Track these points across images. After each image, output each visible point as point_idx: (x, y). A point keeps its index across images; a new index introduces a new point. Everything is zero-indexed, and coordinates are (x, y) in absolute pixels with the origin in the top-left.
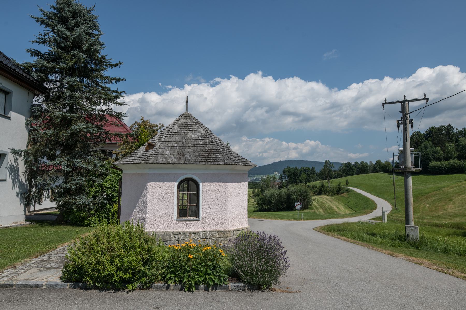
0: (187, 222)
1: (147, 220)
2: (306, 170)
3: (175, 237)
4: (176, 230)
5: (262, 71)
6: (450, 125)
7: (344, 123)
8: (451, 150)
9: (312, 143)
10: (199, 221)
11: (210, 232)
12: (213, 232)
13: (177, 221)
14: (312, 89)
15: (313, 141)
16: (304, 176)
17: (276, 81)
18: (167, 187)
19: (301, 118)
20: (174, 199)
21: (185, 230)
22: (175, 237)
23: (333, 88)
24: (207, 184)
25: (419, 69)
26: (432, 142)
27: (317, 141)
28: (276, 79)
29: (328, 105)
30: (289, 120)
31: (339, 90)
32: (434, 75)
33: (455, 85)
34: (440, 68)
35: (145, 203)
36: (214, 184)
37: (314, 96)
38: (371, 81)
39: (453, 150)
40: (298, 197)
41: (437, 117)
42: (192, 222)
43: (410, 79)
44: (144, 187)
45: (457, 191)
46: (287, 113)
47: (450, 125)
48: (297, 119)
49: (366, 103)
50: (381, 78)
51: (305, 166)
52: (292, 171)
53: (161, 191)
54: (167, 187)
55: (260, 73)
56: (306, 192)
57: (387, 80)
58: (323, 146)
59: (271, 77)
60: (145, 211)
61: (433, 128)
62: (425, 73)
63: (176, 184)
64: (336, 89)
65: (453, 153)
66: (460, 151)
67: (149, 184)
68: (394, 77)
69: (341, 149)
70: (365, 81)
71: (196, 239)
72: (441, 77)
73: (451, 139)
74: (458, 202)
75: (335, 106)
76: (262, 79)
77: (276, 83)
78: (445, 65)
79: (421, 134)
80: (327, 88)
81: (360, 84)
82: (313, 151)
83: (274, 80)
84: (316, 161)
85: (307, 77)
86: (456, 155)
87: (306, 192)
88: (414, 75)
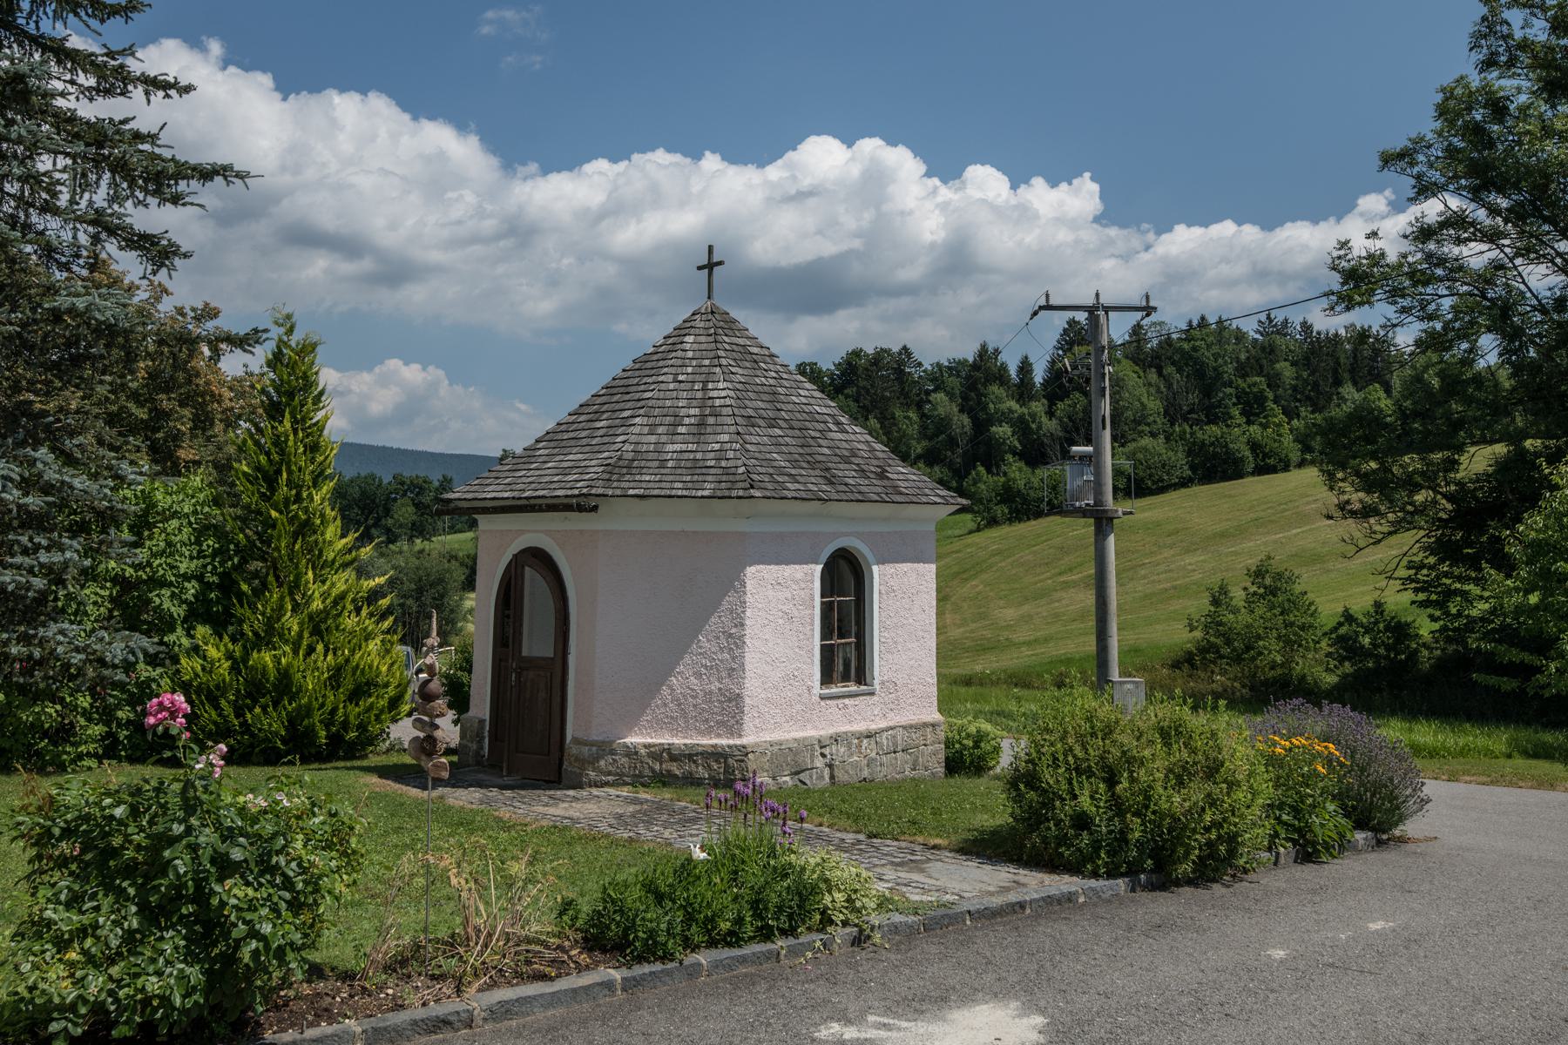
0: (847, 701)
1: (747, 701)
2: (416, 488)
3: (823, 755)
4: (825, 731)
5: (224, 39)
6: (905, 348)
7: (543, 306)
8: (910, 431)
9: (412, 374)
10: (872, 694)
11: (904, 727)
12: (911, 727)
13: (822, 698)
14: (441, 156)
15: (416, 367)
16: (404, 512)
17: (285, 99)
18: (797, 582)
19: (366, 265)
20: (812, 620)
21: (843, 729)
22: (823, 755)
23: (524, 164)
24: (890, 569)
25: (813, 139)
26: (857, 401)
27: (431, 369)
28: (286, 87)
29: (489, 225)
30: (317, 266)
31: (546, 171)
32: (855, 171)
33: (902, 213)
34: (870, 146)
35: (735, 642)
36: (906, 567)
37: (437, 181)
38: (661, 156)
39: (913, 430)
40: (410, 602)
41: (842, 314)
42: (857, 701)
43: (774, 172)
44: (732, 581)
45: (955, 569)
46: (305, 237)
47: (905, 348)
48: (348, 268)
49: (631, 236)
50: (697, 156)
51: (408, 473)
52: (355, 492)
53: (782, 596)
54: (797, 582)
55: (216, 48)
56: (441, 581)
57: (711, 162)
58: (459, 389)
59: (266, 80)
60: (735, 670)
61: (857, 353)
62: (823, 156)
63: (819, 568)
64: (533, 167)
65: (914, 443)
66: (930, 439)
67: (750, 570)
68: (734, 157)
69: (523, 407)
70: (636, 157)
71: (873, 755)
72: (875, 183)
73: (906, 396)
74: (965, 605)
75: (520, 233)
76: (220, 76)
77: (285, 105)
78: (892, 142)
79: (820, 371)
80: (494, 161)
81: (623, 165)
82: (411, 408)
83: (278, 96)
84: (420, 448)
85: (418, 105)
86: (919, 450)
87: (441, 581)
88: (790, 155)
